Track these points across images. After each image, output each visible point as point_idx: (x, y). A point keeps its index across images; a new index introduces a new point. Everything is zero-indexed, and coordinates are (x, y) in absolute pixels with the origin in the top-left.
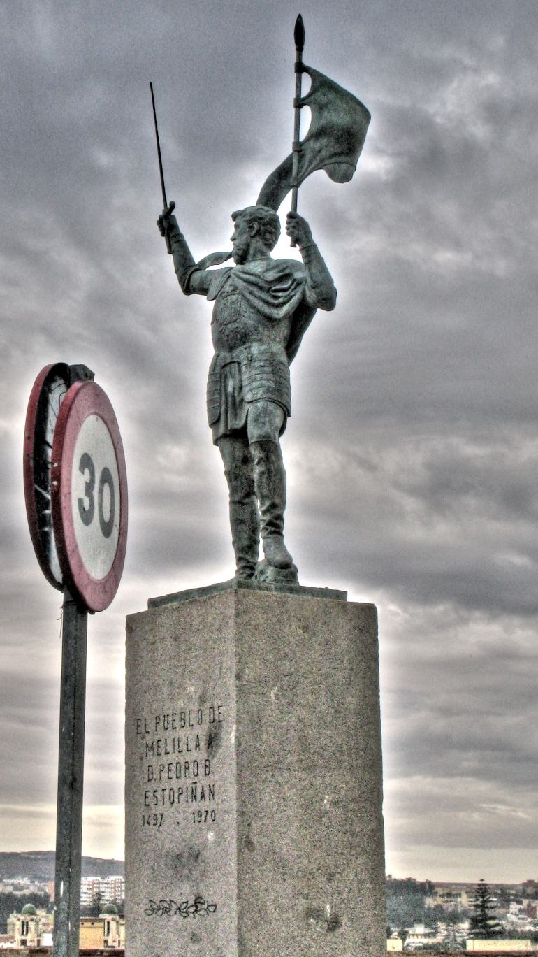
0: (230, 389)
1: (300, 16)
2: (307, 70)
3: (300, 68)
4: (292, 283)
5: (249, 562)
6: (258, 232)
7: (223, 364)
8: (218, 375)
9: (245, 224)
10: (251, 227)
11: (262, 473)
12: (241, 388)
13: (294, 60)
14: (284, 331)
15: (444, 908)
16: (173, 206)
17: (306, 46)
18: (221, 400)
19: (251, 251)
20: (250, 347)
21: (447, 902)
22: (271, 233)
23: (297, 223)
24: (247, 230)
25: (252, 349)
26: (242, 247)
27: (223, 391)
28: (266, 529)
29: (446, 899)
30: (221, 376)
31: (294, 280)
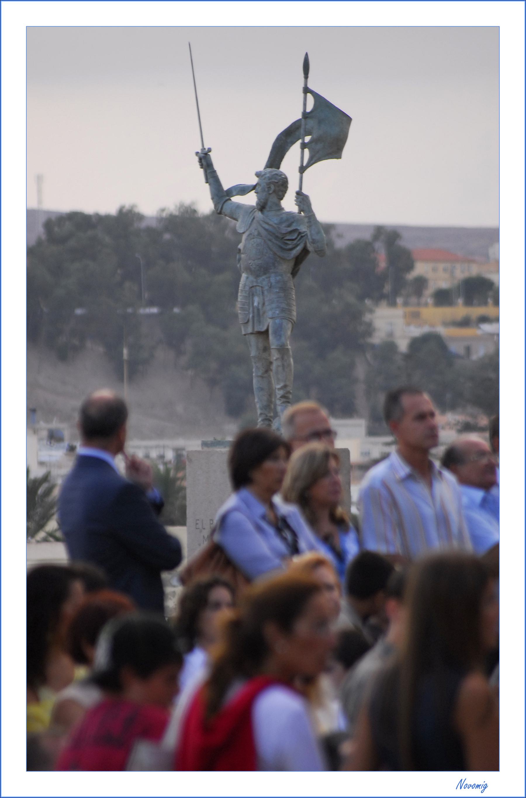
0: (256, 304)
1: (307, 54)
2: (312, 92)
3: (306, 90)
4: (298, 235)
5: (267, 416)
6: (274, 191)
7: (251, 285)
8: (248, 292)
9: (265, 184)
10: (269, 188)
11: (278, 366)
12: (264, 304)
13: (302, 85)
14: (292, 264)
15: (456, 348)
16: (210, 150)
17: (310, 75)
18: (249, 309)
19: (269, 204)
20: (269, 277)
21: (465, 323)
22: (282, 191)
23: (303, 199)
24: (266, 190)
25: (271, 279)
26: (262, 201)
27: (251, 305)
28: (280, 400)
29: (460, 310)
30: (249, 293)
31: (300, 233)
